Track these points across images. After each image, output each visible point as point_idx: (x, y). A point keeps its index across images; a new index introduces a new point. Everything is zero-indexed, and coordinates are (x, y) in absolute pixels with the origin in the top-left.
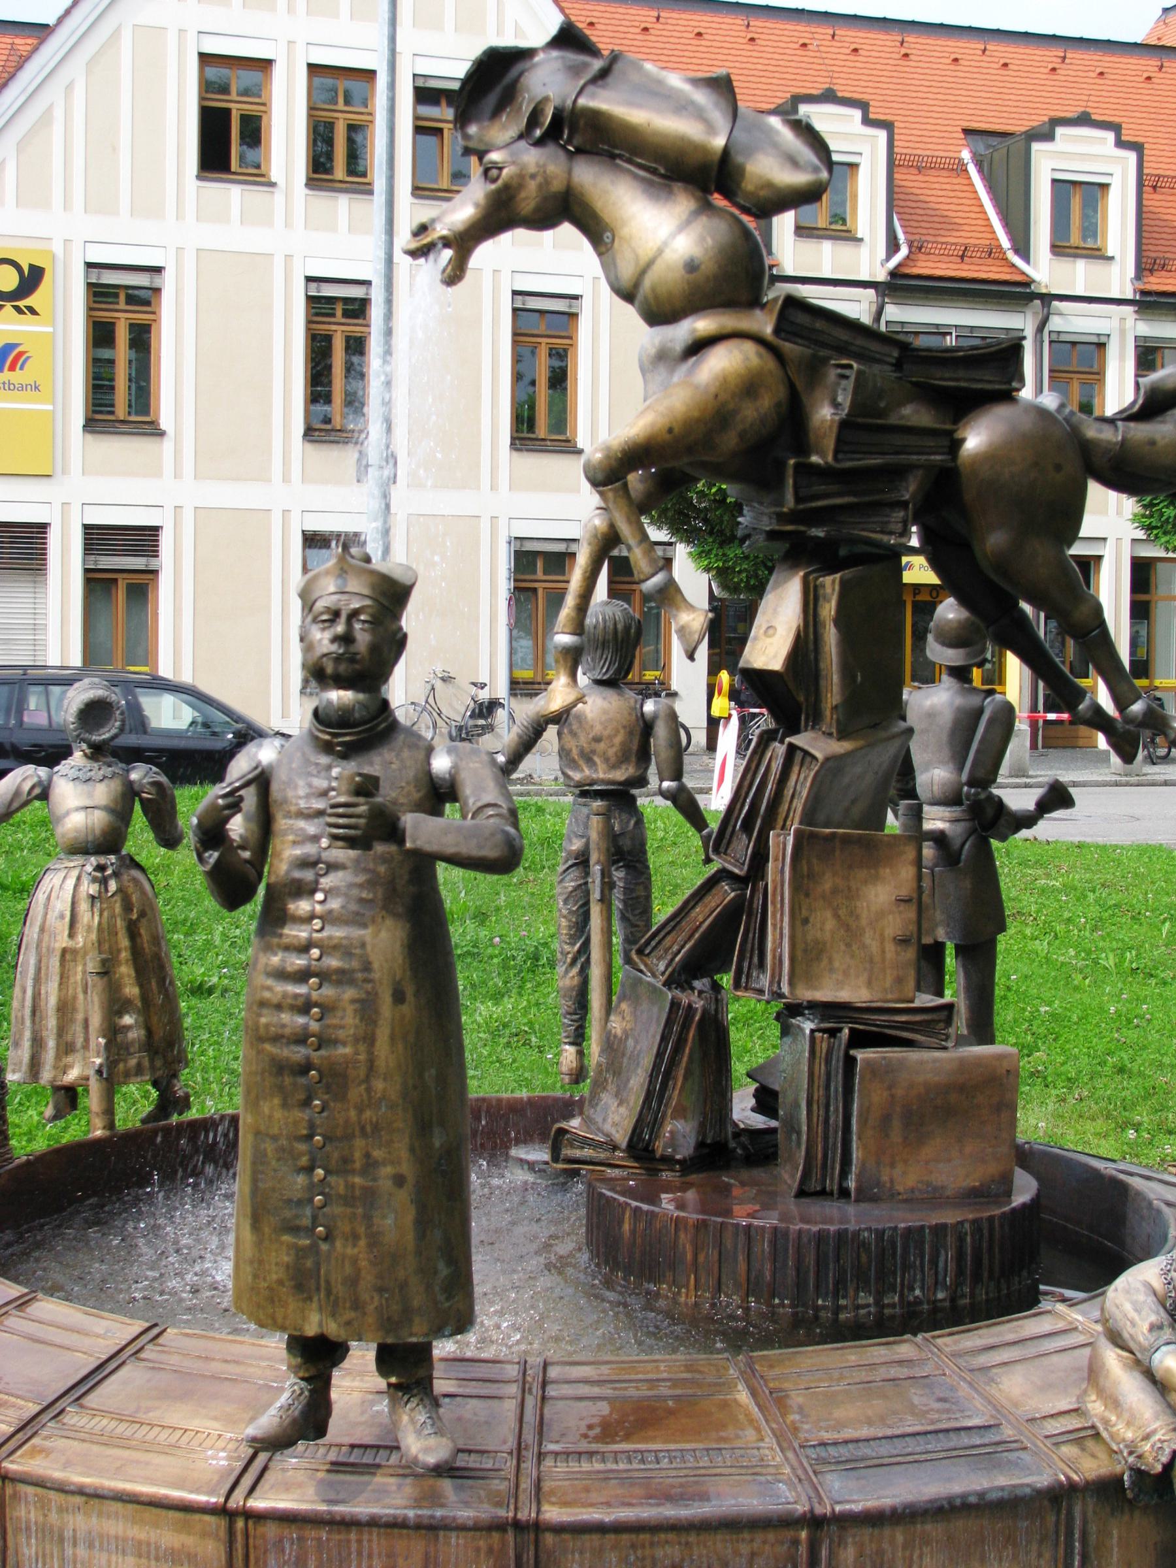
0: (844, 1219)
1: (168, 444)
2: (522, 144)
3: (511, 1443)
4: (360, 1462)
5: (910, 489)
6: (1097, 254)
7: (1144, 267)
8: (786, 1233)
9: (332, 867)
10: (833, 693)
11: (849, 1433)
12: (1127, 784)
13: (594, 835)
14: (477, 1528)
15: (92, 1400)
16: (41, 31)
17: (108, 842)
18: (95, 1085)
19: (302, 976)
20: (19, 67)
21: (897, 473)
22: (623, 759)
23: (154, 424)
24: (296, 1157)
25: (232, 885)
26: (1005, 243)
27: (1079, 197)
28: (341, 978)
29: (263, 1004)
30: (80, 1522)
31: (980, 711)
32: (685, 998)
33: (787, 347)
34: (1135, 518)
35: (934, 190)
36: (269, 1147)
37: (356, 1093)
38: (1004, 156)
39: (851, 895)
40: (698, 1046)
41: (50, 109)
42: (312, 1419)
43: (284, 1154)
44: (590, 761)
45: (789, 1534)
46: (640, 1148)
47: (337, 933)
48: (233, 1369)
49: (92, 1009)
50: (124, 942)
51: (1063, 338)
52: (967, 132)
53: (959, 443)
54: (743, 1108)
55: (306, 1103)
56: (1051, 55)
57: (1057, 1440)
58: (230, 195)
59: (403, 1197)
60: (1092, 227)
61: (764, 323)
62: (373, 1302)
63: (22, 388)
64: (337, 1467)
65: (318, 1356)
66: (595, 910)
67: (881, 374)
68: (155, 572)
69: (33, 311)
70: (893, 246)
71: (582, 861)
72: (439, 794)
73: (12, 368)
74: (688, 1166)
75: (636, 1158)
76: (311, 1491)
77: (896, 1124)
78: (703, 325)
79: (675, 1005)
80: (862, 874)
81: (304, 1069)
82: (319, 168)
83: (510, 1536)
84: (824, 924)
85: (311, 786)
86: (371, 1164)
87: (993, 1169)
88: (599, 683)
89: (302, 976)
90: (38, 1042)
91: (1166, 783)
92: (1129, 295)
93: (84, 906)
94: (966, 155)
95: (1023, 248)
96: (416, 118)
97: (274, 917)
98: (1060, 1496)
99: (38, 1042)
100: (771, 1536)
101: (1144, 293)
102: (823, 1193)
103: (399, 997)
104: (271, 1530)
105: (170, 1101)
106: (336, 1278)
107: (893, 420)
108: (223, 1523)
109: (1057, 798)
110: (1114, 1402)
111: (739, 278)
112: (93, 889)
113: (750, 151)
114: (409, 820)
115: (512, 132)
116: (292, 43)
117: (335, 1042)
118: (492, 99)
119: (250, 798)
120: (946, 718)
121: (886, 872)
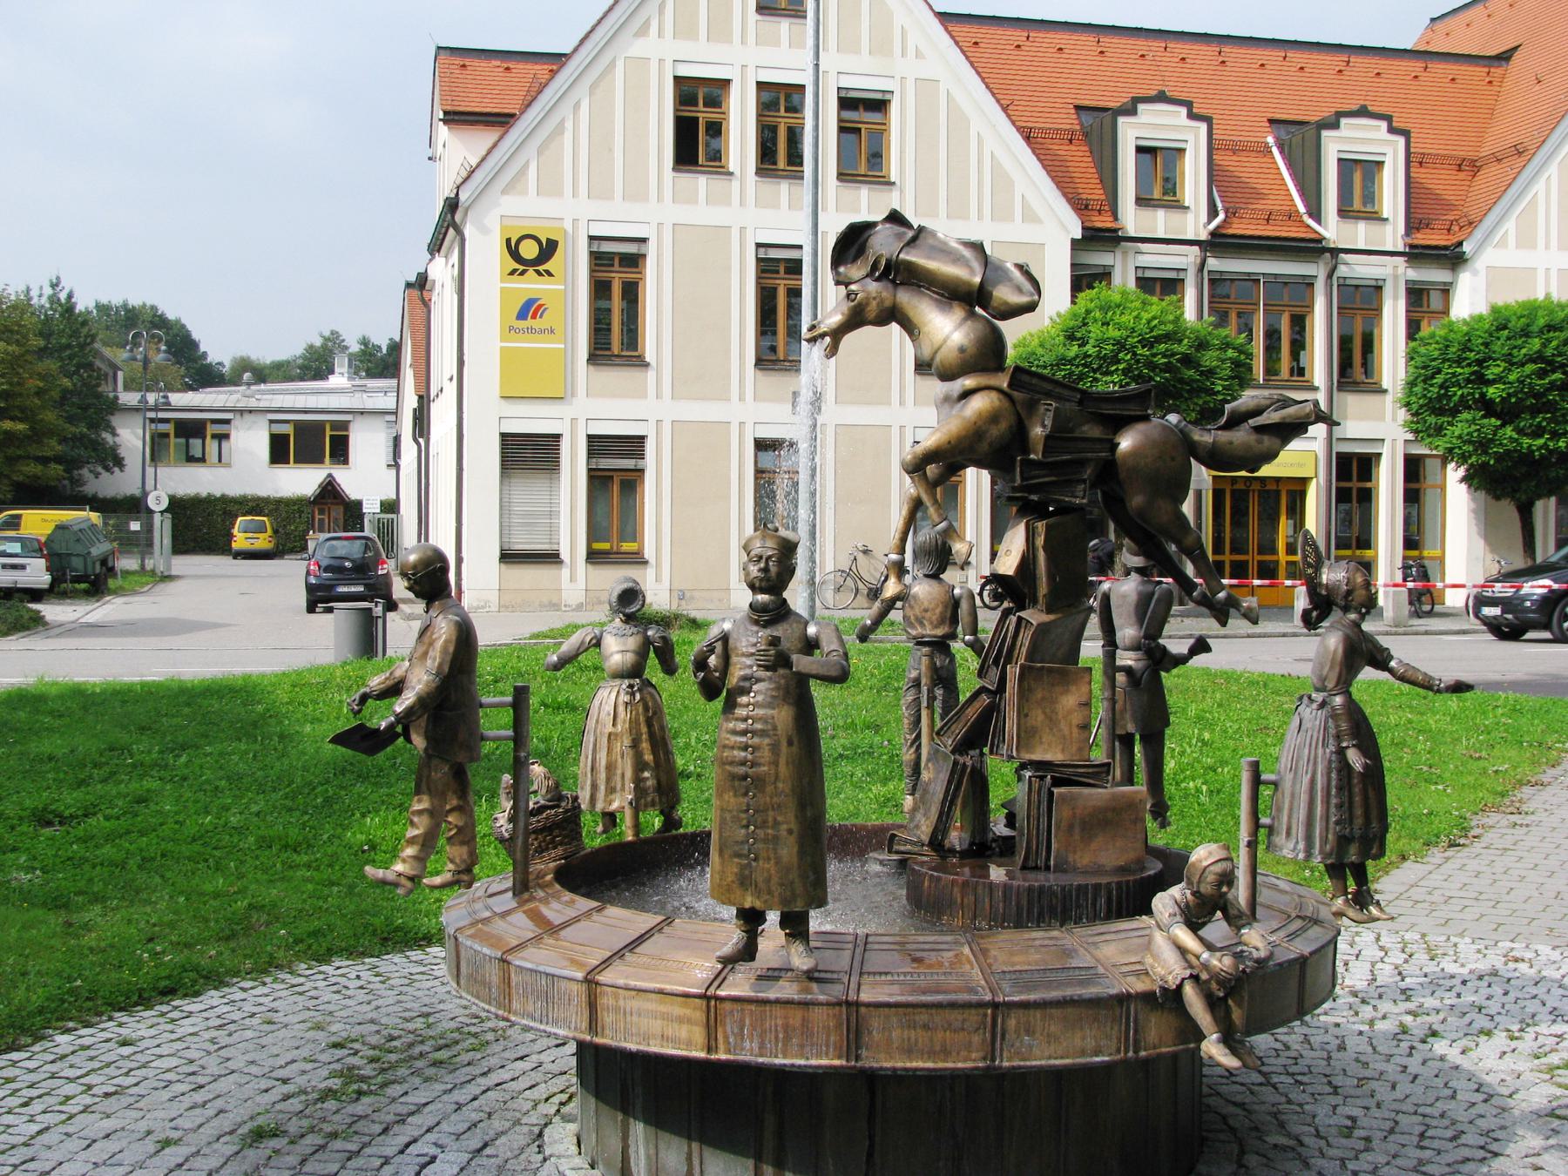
0: (1047, 880)
1: (651, 374)
2: (868, 280)
3: (847, 968)
4: (771, 976)
5: (1088, 473)
6: (1375, 217)
7: (1412, 225)
8: (1011, 887)
9: (758, 680)
10: (1043, 589)
11: (1018, 968)
12: (1396, 634)
13: (923, 668)
14: (828, 1004)
15: (637, 950)
16: (557, 60)
17: (635, 671)
18: (628, 813)
19: (744, 733)
20: (540, 92)
21: (1082, 463)
22: (941, 622)
23: (641, 358)
24: (740, 820)
25: (710, 689)
26: (1302, 209)
27: (1360, 174)
28: (762, 733)
29: (725, 746)
30: (636, 1003)
31: (1153, 594)
32: (961, 760)
33: (1016, 394)
34: (1406, 424)
35: (1243, 168)
36: (728, 816)
37: (769, 789)
38: (1300, 141)
39: (1054, 702)
40: (970, 788)
41: (563, 121)
42: (748, 951)
43: (736, 819)
44: (921, 624)
45: (981, 1011)
46: (936, 842)
47: (760, 712)
48: (709, 937)
49: (626, 767)
50: (644, 729)
51: (1348, 282)
52: (1271, 121)
53: (1114, 446)
54: (1000, 828)
55: (746, 794)
56: (1338, 60)
57: (1125, 974)
58: (700, 182)
59: (792, 840)
60: (1370, 197)
61: (1004, 383)
62: (777, 890)
63: (542, 331)
64: (760, 978)
65: (752, 919)
66: (924, 713)
67: (1071, 407)
68: (642, 471)
69: (549, 274)
70: (1213, 212)
71: (917, 684)
72: (810, 646)
73: (534, 317)
74: (964, 854)
75: (934, 850)
76: (747, 987)
77: (1077, 830)
78: (968, 382)
79: (955, 763)
80: (1058, 689)
81: (745, 777)
82: (766, 154)
83: (844, 1009)
84: (1037, 717)
85: (749, 642)
86: (776, 824)
87: (1132, 855)
88: (927, 576)
89: (744, 733)
90: (594, 787)
91: (1426, 633)
92: (1400, 248)
93: (621, 709)
94: (1270, 140)
95: (1316, 214)
96: (840, 120)
97: (730, 705)
98: (1123, 999)
99: (594, 787)
100: (973, 1011)
101: (1412, 246)
102: (1036, 868)
103: (790, 743)
104: (728, 1006)
105: (671, 822)
106: (760, 879)
107: (1076, 435)
108: (704, 1003)
109: (1201, 646)
110: (1156, 957)
111: (988, 355)
112: (627, 698)
113: (995, 285)
114: (794, 657)
115: (863, 272)
116: (749, 56)
117: (759, 765)
118: (853, 251)
119: (719, 647)
120: (1133, 598)
121: (1073, 688)
